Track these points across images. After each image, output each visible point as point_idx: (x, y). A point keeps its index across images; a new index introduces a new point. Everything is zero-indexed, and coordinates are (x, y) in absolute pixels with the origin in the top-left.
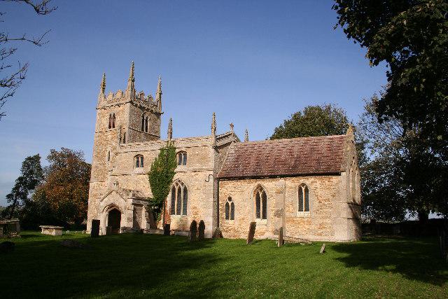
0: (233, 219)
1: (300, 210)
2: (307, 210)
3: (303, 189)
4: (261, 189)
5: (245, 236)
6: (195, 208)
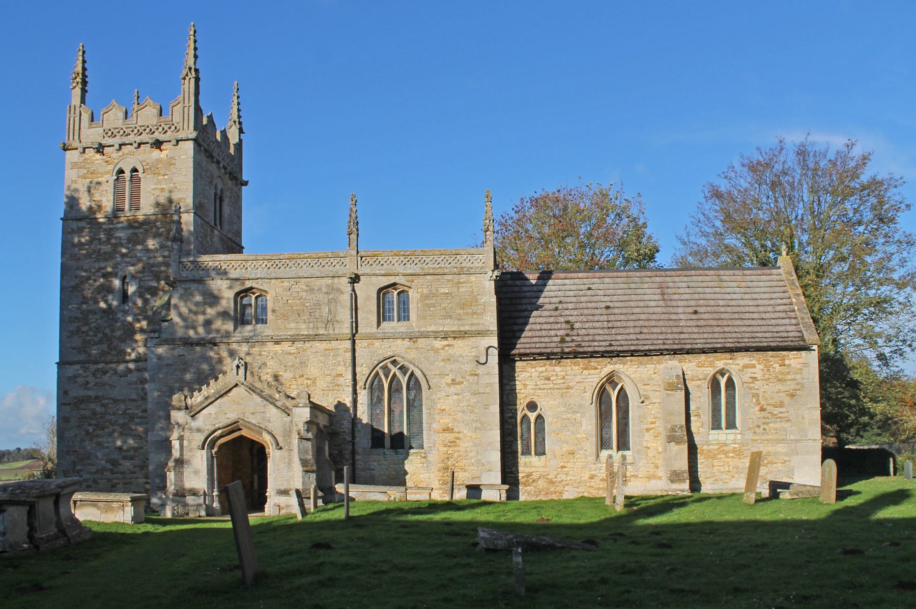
0: (731, 425)
1: (716, 425)
2: (731, 425)
3: (723, 381)
4: (614, 384)
5: (178, 441)
6: (447, 430)
